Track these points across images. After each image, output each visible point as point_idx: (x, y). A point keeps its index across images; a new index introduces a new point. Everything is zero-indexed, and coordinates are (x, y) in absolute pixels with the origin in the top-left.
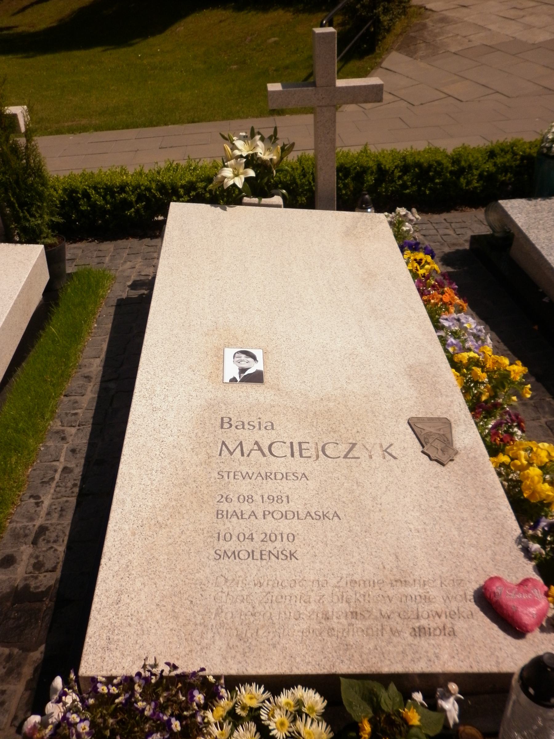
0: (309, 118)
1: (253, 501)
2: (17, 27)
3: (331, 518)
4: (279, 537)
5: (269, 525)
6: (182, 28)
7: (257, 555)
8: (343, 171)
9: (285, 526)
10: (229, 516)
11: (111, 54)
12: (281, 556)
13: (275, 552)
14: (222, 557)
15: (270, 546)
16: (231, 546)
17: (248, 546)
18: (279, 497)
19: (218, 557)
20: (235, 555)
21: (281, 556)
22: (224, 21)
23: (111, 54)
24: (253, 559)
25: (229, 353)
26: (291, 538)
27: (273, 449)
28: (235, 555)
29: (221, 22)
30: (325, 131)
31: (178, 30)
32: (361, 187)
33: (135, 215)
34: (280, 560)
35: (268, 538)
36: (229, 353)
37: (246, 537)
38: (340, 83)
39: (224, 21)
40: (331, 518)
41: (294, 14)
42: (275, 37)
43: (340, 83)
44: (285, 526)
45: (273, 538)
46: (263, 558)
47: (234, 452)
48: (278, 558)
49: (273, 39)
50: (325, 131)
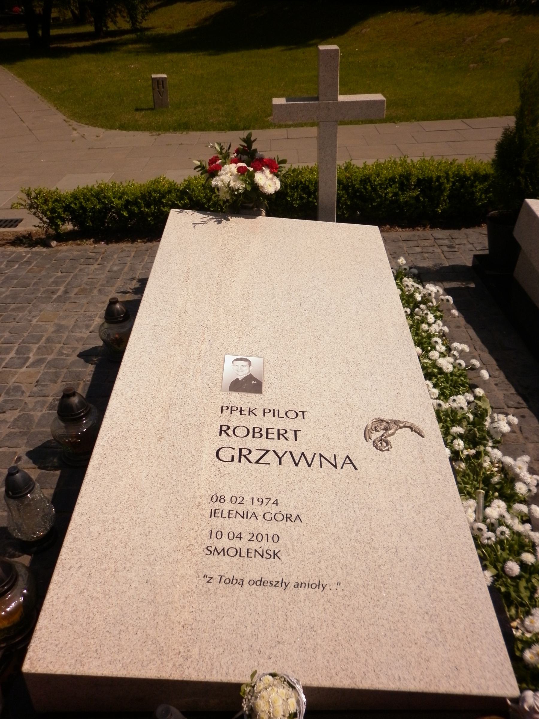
0: (314, 131)
1: (225, 500)
2: (153, 28)
3: (293, 520)
4: (265, 538)
5: (258, 526)
6: (369, 30)
7: (244, 554)
8: (344, 186)
9: (273, 528)
10: (249, 517)
11: (304, 53)
12: (265, 555)
13: (260, 551)
14: (213, 552)
15: (254, 545)
16: (224, 543)
17: (237, 543)
18: (222, 497)
19: (209, 552)
20: (225, 552)
21: (265, 555)
22: (420, 22)
23: (304, 53)
24: (240, 556)
25: (229, 359)
26: (276, 538)
27: (220, 453)
28: (225, 552)
29: (417, 23)
30: (327, 146)
31: (363, 31)
32: (361, 202)
33: (132, 221)
34: (264, 559)
35: (255, 537)
36: (229, 359)
37: (235, 536)
38: (342, 98)
39: (420, 22)
40: (293, 520)
41: (513, 15)
42: (505, 37)
43: (342, 98)
44: (273, 528)
45: (260, 538)
46: (249, 556)
47: (283, 456)
48: (262, 557)
49: (507, 39)
50: (327, 146)
